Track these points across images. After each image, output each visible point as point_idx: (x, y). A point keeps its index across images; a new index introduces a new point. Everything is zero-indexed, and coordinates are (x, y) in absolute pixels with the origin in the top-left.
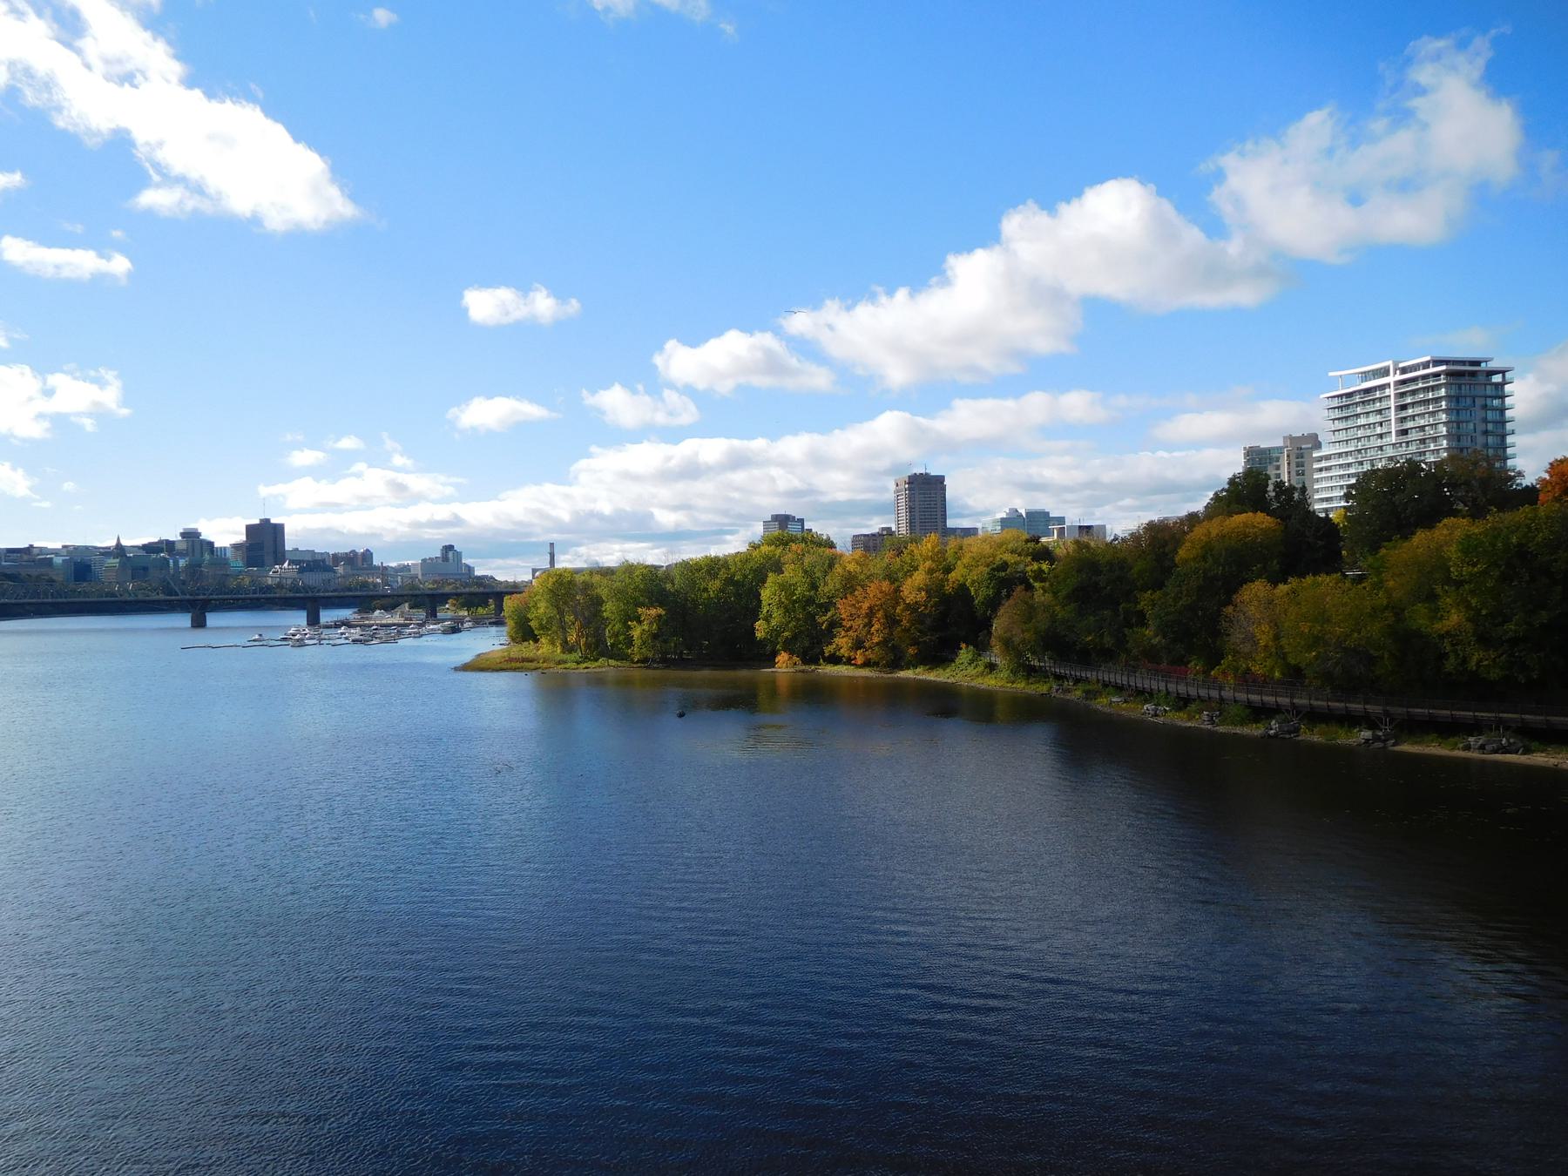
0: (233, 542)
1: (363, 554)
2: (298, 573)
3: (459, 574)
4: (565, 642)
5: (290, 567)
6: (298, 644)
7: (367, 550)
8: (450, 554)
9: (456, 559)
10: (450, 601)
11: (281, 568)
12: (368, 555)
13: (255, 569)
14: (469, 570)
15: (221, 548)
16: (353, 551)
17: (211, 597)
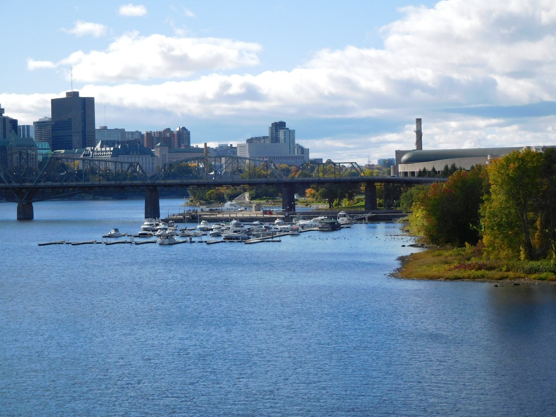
0: (37, 120)
1: (179, 133)
2: (113, 156)
3: (292, 158)
4: (529, 246)
5: (103, 149)
6: (167, 241)
7: (184, 129)
8: (281, 133)
9: (287, 140)
10: (308, 191)
11: (93, 151)
12: (184, 134)
13: (63, 151)
14: (302, 153)
15: (24, 126)
16: (168, 130)
17: (39, 184)
